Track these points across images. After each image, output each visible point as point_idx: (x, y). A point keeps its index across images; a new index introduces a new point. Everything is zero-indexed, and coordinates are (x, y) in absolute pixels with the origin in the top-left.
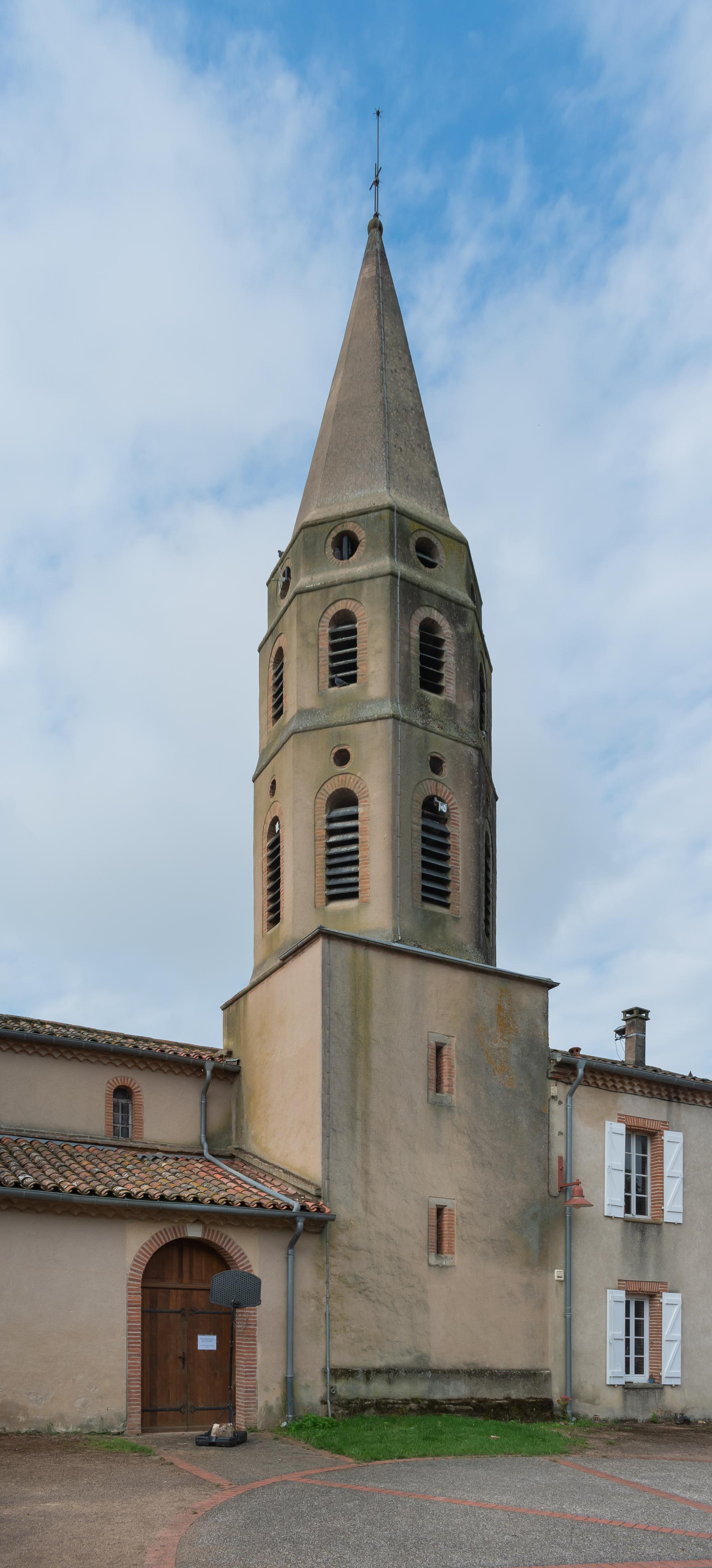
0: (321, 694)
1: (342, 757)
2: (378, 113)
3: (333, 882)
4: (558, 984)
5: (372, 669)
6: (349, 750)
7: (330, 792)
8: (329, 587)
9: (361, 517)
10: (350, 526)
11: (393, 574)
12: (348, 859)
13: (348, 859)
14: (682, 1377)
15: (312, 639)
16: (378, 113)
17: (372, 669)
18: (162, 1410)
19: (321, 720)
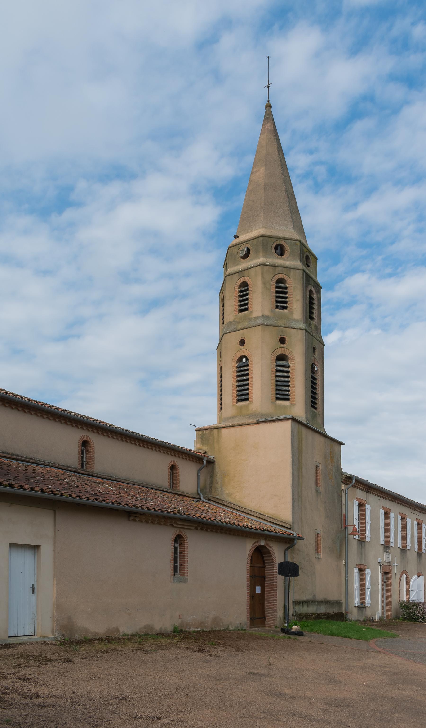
0: (272, 311)
1: (282, 341)
2: (268, 57)
3: (278, 392)
4: (344, 444)
5: (295, 307)
6: (286, 338)
7: (278, 354)
8: (276, 266)
9: (287, 241)
10: (282, 243)
11: (303, 270)
12: (285, 384)
13: (285, 384)
14: (371, 604)
15: (268, 286)
16: (268, 57)
17: (295, 307)
18: (261, 618)
19: (274, 322)
